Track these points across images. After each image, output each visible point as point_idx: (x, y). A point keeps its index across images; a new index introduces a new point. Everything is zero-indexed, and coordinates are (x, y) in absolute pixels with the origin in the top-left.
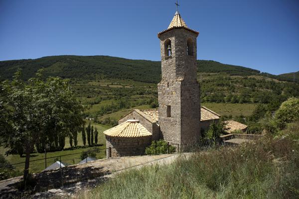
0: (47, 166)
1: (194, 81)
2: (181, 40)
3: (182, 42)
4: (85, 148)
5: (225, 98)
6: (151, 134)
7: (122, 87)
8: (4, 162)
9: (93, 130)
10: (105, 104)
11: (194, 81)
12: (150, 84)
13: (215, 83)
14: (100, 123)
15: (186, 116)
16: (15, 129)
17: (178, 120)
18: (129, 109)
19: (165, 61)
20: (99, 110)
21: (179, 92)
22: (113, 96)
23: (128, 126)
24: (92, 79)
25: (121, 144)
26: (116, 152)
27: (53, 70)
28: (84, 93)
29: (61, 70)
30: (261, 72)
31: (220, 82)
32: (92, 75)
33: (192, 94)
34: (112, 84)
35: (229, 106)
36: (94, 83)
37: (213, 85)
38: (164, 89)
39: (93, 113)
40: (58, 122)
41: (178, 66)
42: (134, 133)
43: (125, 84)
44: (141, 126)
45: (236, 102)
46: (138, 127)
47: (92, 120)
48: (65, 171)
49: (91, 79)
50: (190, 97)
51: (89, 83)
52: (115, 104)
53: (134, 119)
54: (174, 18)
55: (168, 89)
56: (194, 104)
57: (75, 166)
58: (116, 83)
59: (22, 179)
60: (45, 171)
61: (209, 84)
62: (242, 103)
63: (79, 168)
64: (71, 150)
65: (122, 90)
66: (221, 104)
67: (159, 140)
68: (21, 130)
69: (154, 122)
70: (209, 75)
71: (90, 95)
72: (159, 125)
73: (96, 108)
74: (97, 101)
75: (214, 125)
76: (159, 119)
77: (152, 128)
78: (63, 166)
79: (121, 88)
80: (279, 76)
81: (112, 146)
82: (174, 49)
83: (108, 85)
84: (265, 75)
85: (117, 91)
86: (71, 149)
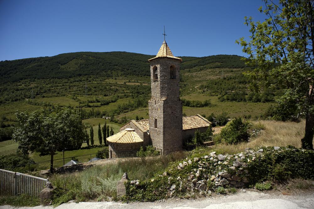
0: (65, 163)
1: (176, 99)
2: (165, 67)
3: (165, 69)
4: (101, 147)
5: (246, 96)
6: (142, 141)
7: (139, 84)
8: (28, 160)
9: (108, 130)
10: (122, 102)
11: (176, 99)
13: (237, 80)
14: (116, 122)
15: (168, 128)
16: (46, 143)
17: (161, 131)
18: (146, 108)
19: (153, 83)
20: (116, 108)
21: (162, 109)
22: (131, 94)
23: (125, 134)
24: (109, 76)
26: (115, 154)
27: (70, 68)
28: (101, 91)
29: (77, 67)
31: (242, 80)
32: (109, 72)
33: (174, 110)
34: (130, 82)
35: (250, 104)
36: (111, 81)
37: (235, 82)
38: (153, 106)
39: (110, 112)
40: (69, 138)
41: (162, 88)
42: (129, 140)
43: (142, 82)
44: (136, 134)
45: (258, 100)
46: (133, 135)
47: (108, 119)
48: (75, 167)
49: (108, 77)
50: (172, 113)
51: (106, 80)
52: (132, 102)
53: (131, 128)
54: (162, 46)
55: (155, 106)
56: (176, 117)
57: (82, 164)
58: (133, 81)
59: (49, 171)
60: (62, 167)
61: (231, 82)
62: (264, 102)
63: (85, 166)
64: (88, 149)
65: (139, 88)
66: (242, 103)
67: (148, 146)
68: (49, 143)
69: (145, 131)
70: (232, 71)
71: (107, 93)
72: (149, 134)
73: (112, 107)
74: (114, 100)
75: (198, 133)
76: (150, 129)
77: (143, 136)
78: (75, 163)
79: (139, 86)
81: (112, 150)
82: (159, 74)
83: (125, 83)
85: (134, 88)
86: (88, 148)
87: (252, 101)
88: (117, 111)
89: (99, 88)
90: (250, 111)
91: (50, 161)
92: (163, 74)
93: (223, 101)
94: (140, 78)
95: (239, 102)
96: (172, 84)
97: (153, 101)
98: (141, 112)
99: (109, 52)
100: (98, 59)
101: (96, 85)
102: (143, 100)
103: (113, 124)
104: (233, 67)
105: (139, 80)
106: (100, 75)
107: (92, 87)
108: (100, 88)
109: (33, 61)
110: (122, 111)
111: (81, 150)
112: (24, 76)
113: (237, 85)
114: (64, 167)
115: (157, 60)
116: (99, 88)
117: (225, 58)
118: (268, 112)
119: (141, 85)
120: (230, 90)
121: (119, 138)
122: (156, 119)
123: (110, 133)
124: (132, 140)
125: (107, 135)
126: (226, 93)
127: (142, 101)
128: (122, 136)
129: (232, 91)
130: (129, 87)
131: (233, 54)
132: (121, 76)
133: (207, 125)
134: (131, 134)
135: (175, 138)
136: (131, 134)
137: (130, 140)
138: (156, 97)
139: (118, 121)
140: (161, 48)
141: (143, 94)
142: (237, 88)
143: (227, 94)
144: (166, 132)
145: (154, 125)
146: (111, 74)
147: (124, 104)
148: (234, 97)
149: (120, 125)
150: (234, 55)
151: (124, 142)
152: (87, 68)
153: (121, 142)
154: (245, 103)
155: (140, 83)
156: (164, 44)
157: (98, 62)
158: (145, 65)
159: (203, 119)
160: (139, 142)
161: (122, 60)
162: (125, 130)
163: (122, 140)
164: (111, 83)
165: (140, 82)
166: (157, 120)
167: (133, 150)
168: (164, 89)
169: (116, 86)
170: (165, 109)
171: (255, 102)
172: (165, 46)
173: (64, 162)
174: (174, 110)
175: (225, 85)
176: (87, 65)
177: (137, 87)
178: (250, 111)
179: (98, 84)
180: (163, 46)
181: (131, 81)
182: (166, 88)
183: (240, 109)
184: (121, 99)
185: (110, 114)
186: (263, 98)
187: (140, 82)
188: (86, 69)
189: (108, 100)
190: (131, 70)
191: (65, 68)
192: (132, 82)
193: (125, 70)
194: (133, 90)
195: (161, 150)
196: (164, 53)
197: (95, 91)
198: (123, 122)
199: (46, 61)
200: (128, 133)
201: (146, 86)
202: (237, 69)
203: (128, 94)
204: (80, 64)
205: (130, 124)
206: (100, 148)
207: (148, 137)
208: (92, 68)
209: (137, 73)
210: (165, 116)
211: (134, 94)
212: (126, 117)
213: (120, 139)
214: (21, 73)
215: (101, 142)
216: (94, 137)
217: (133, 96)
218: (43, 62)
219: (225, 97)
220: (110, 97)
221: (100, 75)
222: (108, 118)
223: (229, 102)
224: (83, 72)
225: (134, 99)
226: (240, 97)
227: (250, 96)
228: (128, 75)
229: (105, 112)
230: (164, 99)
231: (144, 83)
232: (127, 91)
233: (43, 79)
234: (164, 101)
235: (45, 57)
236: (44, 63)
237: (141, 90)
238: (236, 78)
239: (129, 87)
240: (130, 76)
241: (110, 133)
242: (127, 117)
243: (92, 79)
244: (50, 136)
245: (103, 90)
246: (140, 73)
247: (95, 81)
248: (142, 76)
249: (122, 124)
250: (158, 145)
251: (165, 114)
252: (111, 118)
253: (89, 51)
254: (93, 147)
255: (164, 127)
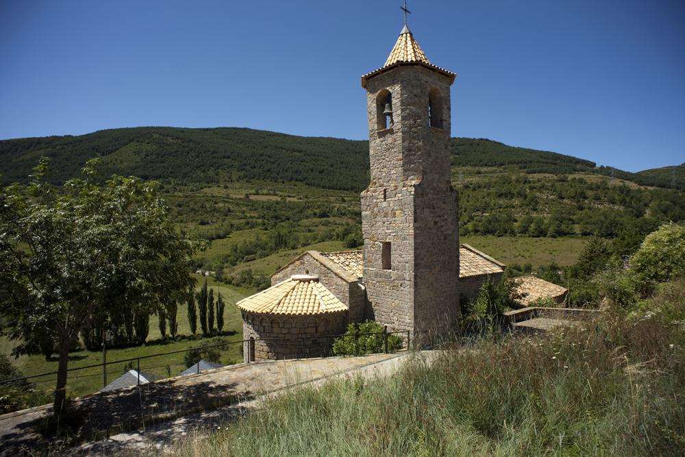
0: (108, 381)
1: (443, 187)
2: (415, 92)
7: (279, 199)
8: (9, 373)
9: (212, 299)
10: (239, 239)
12: (344, 194)
13: (492, 190)
14: (228, 282)
17: (407, 276)
18: (295, 251)
19: (378, 141)
20: (227, 252)
21: (409, 211)
22: (260, 221)
23: (293, 289)
24: (210, 181)
25: (276, 330)
26: (266, 348)
28: (192, 214)
29: (138, 159)
30: (598, 165)
32: (211, 173)
33: (440, 216)
34: (257, 194)
35: (523, 242)
36: (216, 191)
37: (489, 195)
40: (134, 279)
41: (408, 152)
42: (306, 305)
43: (286, 194)
44: (324, 288)
45: (541, 233)
48: (148, 393)
49: (208, 183)
50: (436, 223)
51: (205, 190)
52: (264, 238)
53: (307, 272)
54: (399, 41)
55: (385, 204)
57: (171, 382)
58: (265, 191)
59: (50, 410)
61: (479, 194)
62: (554, 237)
65: (278, 207)
68: (49, 299)
69: (353, 279)
72: (363, 288)
74: (222, 233)
76: (364, 272)
77: (347, 295)
79: (277, 203)
80: (639, 174)
81: (256, 336)
82: (399, 112)
83: (247, 196)
84: (607, 171)
85: (268, 208)
86: (163, 341)
87: (527, 235)
88: (230, 258)
89: (188, 206)
90: (527, 255)
91: (56, 375)
92: (410, 109)
93: (464, 236)
94: (280, 186)
95: (499, 236)
96: (433, 142)
97: (375, 191)
98: (284, 259)
99: (211, 127)
100: (187, 144)
101: (183, 199)
102: (288, 234)
103: (222, 285)
104: (482, 163)
105: (278, 191)
106: (192, 178)
107: (173, 204)
108: (191, 206)
109: (36, 146)
110: (240, 259)
111: (147, 348)
112: (11, 178)
113: (493, 201)
114: (107, 394)
115: (391, 71)
116: (188, 206)
117: (463, 145)
118: (591, 252)
119: (282, 201)
120: (478, 210)
121: (278, 301)
122: (390, 243)
123: (215, 305)
124: (317, 305)
125: (208, 310)
126: (471, 218)
127: (286, 235)
128: (287, 296)
129: (483, 213)
130: (256, 206)
131: (480, 137)
132: (238, 181)
133: (494, 268)
134: (310, 289)
135: (442, 299)
136: (310, 289)
137: (311, 304)
138: (387, 180)
139: (233, 279)
140: (396, 46)
141: (287, 222)
142: (494, 207)
143: (473, 219)
144: (421, 278)
145: (380, 262)
146: (216, 177)
147: (246, 243)
148: (490, 227)
149: (238, 288)
150: (482, 139)
151: (294, 312)
152: (162, 162)
153: (284, 312)
154: (513, 239)
155: (281, 196)
156: (404, 35)
157: (186, 149)
158: (291, 157)
159: (482, 256)
160: (336, 310)
161: (241, 146)
162: (290, 279)
163: (286, 305)
164: (216, 196)
165: (281, 193)
166: (390, 249)
167: (318, 334)
168: (415, 155)
169: (227, 202)
170: (418, 211)
171: (534, 237)
172: (409, 38)
173: (105, 378)
174: (440, 216)
175: (468, 201)
176: (162, 157)
177: (274, 205)
178: (527, 255)
179: (186, 197)
180: (404, 39)
181: (260, 191)
182: (419, 150)
183: (504, 251)
184: (238, 232)
185: (214, 265)
186: (551, 229)
187: (281, 193)
188: (158, 165)
189: (209, 234)
190: (260, 167)
191: (111, 161)
192: (263, 194)
193: (248, 167)
194: (265, 212)
195: (409, 333)
196: (409, 53)
197: (180, 214)
198: (244, 282)
199: (66, 144)
200: (301, 286)
201: (294, 202)
202: (490, 169)
203: (254, 220)
204: (144, 154)
205: (302, 263)
206: (192, 342)
207: (361, 296)
208: (173, 164)
209: (274, 175)
210: (418, 232)
211: (268, 220)
212: (250, 270)
213: (279, 304)
214: (6, 171)
215: (194, 328)
216: (177, 316)
217: (264, 225)
218: (60, 147)
219: (470, 226)
220: (213, 227)
221: (192, 178)
222: (210, 273)
223: (479, 237)
224: (153, 170)
225: (268, 231)
226: (502, 226)
227: (524, 224)
228: (253, 178)
229: (203, 259)
230: (413, 183)
231: (290, 197)
232: (252, 215)
233: (58, 185)
234: (414, 186)
235: (65, 136)
236: (63, 148)
237: (283, 212)
238: (490, 186)
239: (256, 206)
240: (258, 182)
241: (215, 306)
242: (253, 271)
243: (172, 186)
244: (55, 271)
245: (198, 211)
246: (281, 175)
247: (179, 191)
248: (285, 181)
249: (241, 286)
250: (395, 318)
251: (418, 225)
252: (216, 274)
253: (166, 126)
254: (174, 339)
255: (416, 265)
